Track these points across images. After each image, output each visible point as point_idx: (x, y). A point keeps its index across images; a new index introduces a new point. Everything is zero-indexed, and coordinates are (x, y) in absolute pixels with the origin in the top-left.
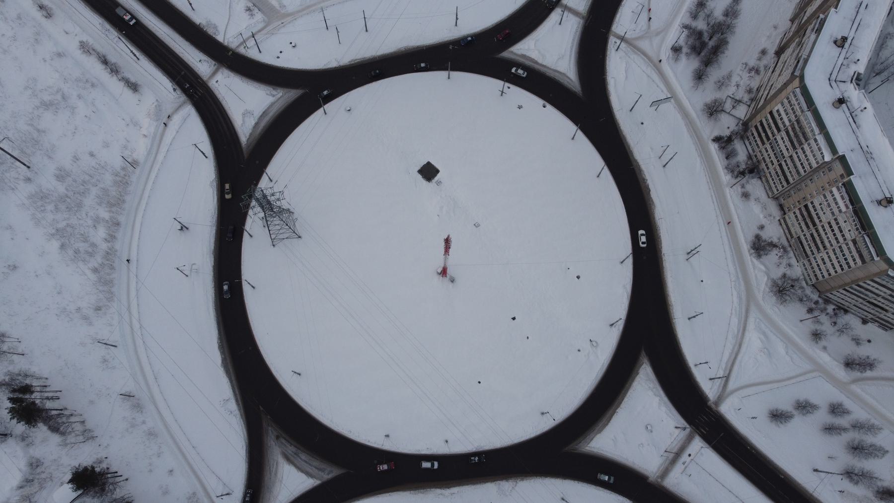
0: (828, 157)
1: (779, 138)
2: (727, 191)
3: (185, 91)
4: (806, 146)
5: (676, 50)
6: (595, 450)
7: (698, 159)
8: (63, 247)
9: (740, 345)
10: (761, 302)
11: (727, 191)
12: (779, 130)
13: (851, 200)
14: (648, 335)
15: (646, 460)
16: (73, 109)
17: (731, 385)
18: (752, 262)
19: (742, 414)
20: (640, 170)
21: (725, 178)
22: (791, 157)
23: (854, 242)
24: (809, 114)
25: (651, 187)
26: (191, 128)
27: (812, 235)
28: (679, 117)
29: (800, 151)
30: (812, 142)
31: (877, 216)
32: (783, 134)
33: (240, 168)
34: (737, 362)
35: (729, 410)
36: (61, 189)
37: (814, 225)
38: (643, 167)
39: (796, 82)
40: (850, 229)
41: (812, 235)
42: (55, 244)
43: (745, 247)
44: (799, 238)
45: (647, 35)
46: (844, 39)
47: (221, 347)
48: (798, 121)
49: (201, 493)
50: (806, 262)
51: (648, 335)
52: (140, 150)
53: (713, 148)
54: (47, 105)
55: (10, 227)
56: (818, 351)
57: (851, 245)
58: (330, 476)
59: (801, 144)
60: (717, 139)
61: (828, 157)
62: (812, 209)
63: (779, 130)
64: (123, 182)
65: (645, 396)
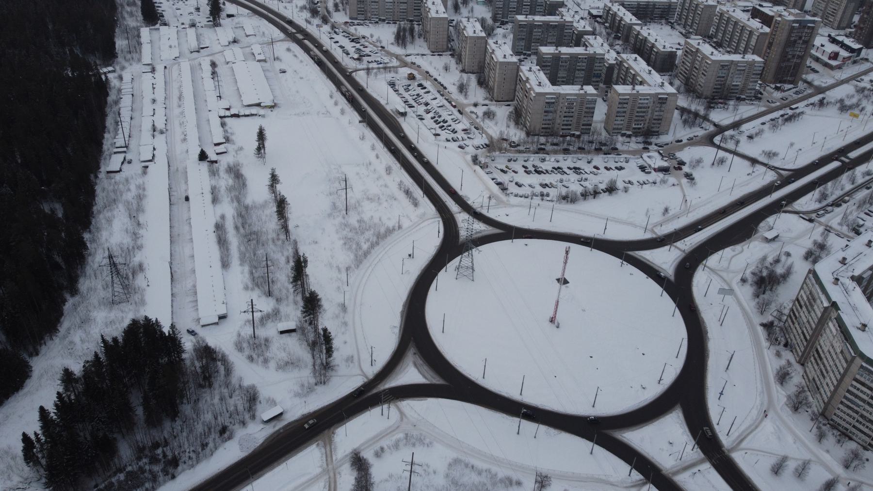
0: (826, 304)
1: (802, 314)
2: (766, 351)
5: (744, 281)
6: (625, 440)
7: (747, 331)
8: (345, 244)
9: (756, 427)
10: (779, 411)
11: (766, 351)
13: (839, 326)
14: (687, 394)
15: (665, 461)
16: (380, 204)
17: (744, 445)
18: (777, 391)
20: (704, 322)
21: (765, 344)
24: (817, 286)
25: (709, 331)
28: (738, 309)
31: (856, 335)
33: (452, 247)
34: (754, 433)
35: (739, 458)
36: (357, 225)
37: (821, 359)
39: (832, 326)
42: (342, 242)
44: (814, 379)
45: (727, 270)
47: (404, 306)
48: (809, 312)
49: (356, 358)
50: (818, 396)
51: (687, 394)
52: (406, 224)
54: (368, 199)
55: (324, 229)
56: (821, 451)
57: (840, 356)
58: (438, 383)
60: (763, 325)
62: (821, 352)
64: (389, 231)
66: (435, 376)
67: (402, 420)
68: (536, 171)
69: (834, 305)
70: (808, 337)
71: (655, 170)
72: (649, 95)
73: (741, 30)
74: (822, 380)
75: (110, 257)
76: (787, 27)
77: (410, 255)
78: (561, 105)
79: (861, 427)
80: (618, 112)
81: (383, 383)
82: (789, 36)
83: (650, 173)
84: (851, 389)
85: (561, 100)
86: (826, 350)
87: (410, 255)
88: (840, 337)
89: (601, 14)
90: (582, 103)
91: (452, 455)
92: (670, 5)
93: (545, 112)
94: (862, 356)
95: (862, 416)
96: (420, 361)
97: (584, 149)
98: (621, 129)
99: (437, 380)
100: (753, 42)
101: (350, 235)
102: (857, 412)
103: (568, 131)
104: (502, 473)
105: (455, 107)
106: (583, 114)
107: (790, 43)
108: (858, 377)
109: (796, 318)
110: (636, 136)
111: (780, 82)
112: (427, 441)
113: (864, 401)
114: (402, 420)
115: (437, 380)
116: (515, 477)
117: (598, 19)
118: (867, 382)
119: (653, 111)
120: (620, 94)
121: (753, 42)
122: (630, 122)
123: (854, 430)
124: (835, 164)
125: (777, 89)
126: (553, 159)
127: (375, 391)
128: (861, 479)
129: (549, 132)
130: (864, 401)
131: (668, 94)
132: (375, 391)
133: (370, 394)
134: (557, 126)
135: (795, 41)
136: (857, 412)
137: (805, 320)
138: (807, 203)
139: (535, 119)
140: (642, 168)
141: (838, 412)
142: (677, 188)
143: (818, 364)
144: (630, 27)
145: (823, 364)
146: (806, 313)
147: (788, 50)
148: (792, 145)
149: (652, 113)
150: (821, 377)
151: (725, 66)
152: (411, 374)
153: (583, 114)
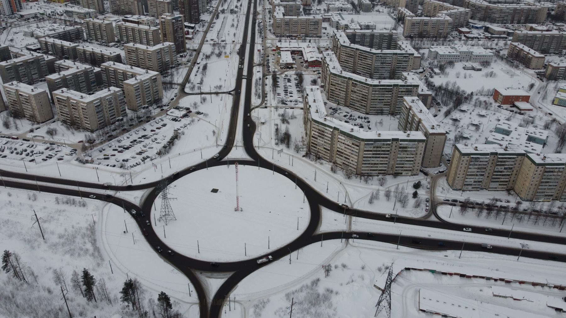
1: (319, 141)
3: (104, 200)
4: (326, 134)
6: (323, 232)
8: (72, 255)
12: (317, 138)
19: (358, 206)
22: (325, 142)
23: (353, 144)
26: (119, 210)
27: (345, 157)
29: (325, 137)
30: (326, 131)
32: (319, 138)
37: (342, 153)
38: (323, 224)
40: (349, 142)
41: (345, 157)
43: (331, 173)
44: (343, 163)
46: (315, 100)
48: (323, 138)
52: (96, 219)
53: (304, 158)
57: (353, 146)
58: (230, 275)
59: (323, 135)
60: (304, 156)
61: (331, 130)
63: (317, 138)
65: (327, 214)
66: (225, 274)
67: (241, 304)
68: (124, 148)
69: (335, 128)
70: (329, 149)
71: (181, 117)
72: (147, 79)
73: (139, 32)
74: (348, 161)
75: (466, 138)
76: (171, 23)
77: (125, 232)
78: (104, 104)
79: (373, 169)
80: (136, 96)
81: (208, 299)
82: (173, 28)
83: (180, 120)
84: (364, 156)
85: (103, 102)
86: (343, 148)
87: (125, 232)
88: (348, 139)
89: (39, 47)
90: (115, 98)
91: (283, 295)
92: (78, 30)
93: (97, 113)
94: (363, 140)
95: (372, 164)
96: (209, 274)
97: (132, 125)
98: (141, 105)
99: (229, 275)
100: (151, 37)
101: (67, 248)
102: (369, 164)
103: (114, 119)
104: (308, 282)
105: (17, 139)
106: (119, 105)
107: (175, 31)
108: (365, 149)
109: (316, 145)
110: (151, 105)
111: (181, 53)
112: (265, 300)
113: (370, 157)
114: (241, 304)
115: (229, 275)
116: (314, 278)
117: (38, 51)
118: (369, 149)
119: (153, 88)
120: (133, 85)
121: (151, 37)
122: (144, 99)
123: (371, 172)
124: (244, 82)
125: (182, 56)
126: (125, 138)
127: (209, 305)
128: (388, 186)
129: (103, 125)
130: (370, 157)
131: (155, 76)
132: (209, 305)
133: (209, 309)
134: (107, 119)
135: (177, 29)
136: (369, 164)
137: (323, 143)
138: (255, 101)
139: (91, 120)
140: (175, 120)
141: (363, 168)
142: (201, 121)
143: (342, 156)
144: (74, 49)
145: (345, 154)
146: (321, 139)
147: (176, 35)
148: (220, 79)
149: (153, 90)
150: (347, 160)
151: (160, 52)
152: (214, 284)
153: (119, 105)
